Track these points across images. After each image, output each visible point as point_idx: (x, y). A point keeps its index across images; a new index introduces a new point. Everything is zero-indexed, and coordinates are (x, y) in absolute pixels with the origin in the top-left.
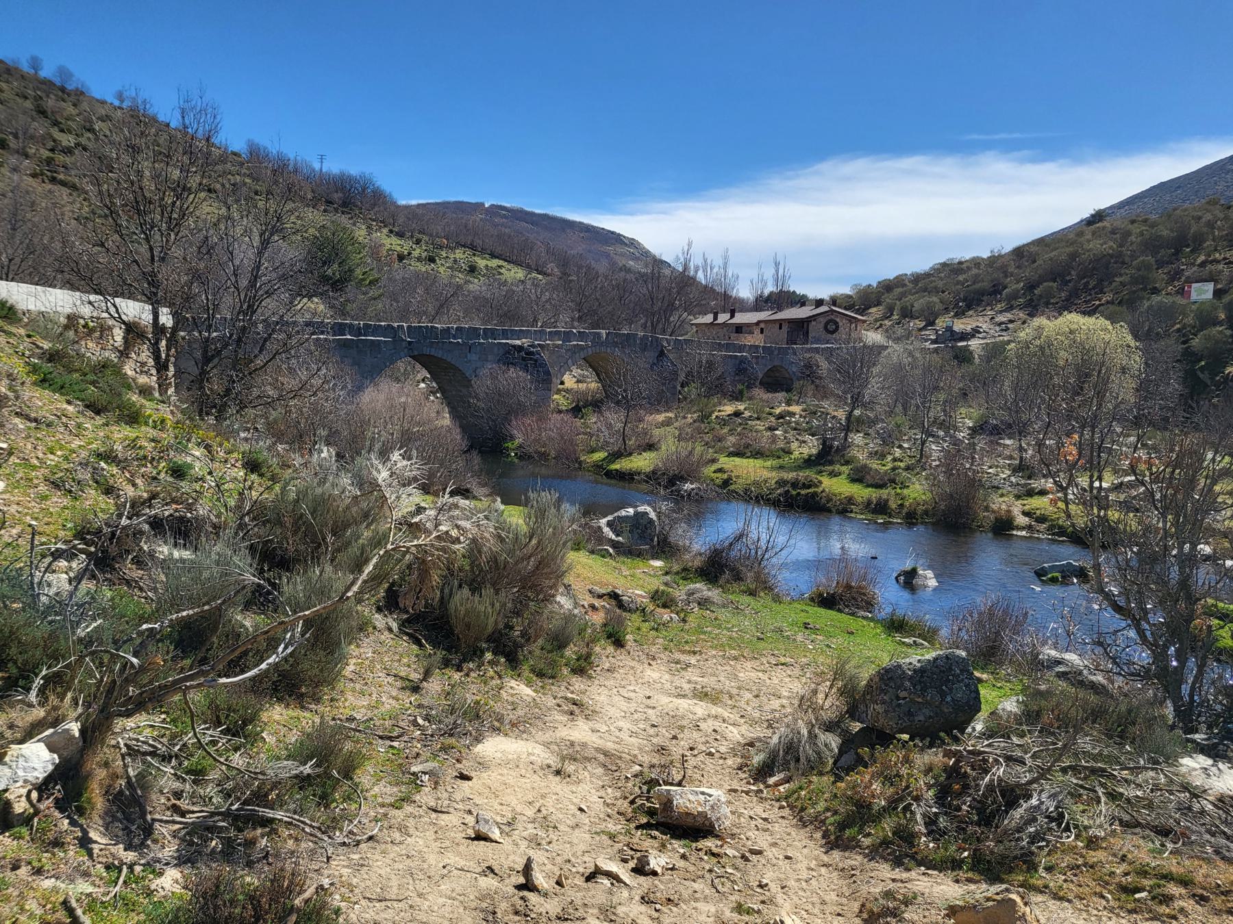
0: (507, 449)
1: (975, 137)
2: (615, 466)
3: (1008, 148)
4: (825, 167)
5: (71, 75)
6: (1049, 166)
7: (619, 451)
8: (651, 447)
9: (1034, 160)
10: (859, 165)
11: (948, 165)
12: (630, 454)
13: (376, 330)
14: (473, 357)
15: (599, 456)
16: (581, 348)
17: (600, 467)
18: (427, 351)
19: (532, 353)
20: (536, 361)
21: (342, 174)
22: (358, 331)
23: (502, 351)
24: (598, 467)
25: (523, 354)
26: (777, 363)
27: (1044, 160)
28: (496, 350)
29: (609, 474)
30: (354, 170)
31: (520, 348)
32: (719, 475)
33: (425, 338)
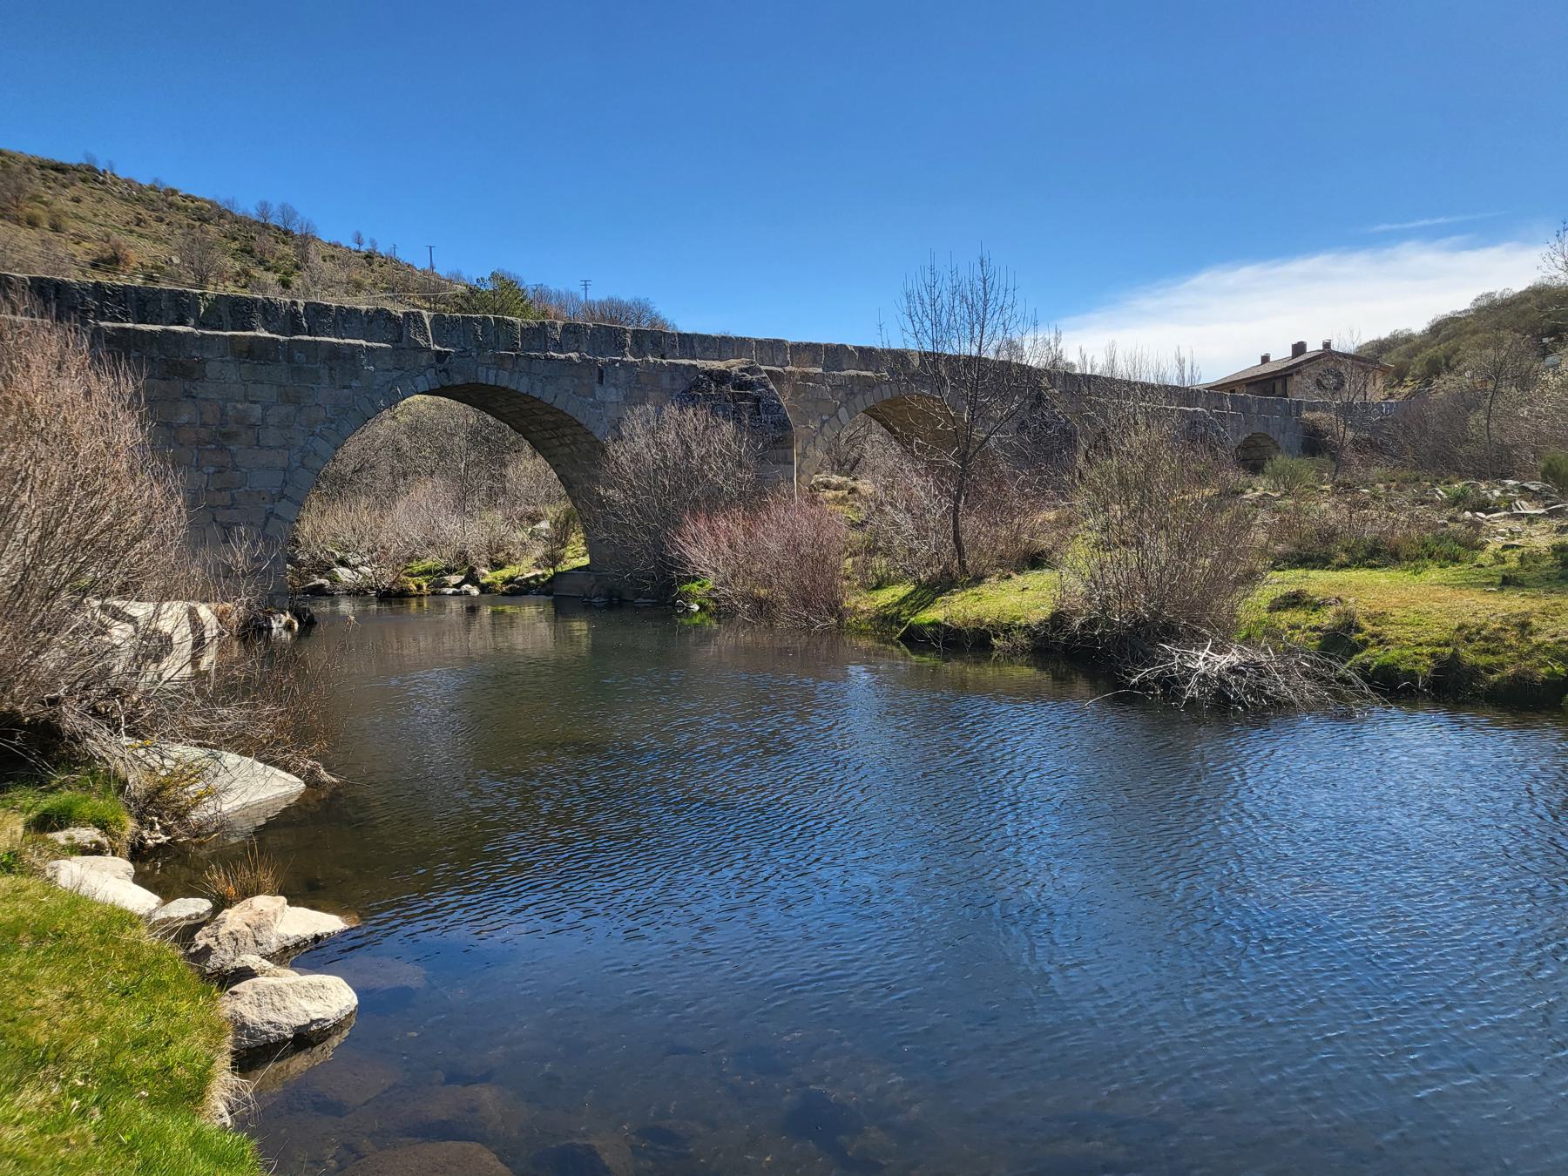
0: (687, 596)
1: (1385, 227)
2: (934, 614)
3: (1432, 235)
4: (1203, 279)
5: (295, 213)
6: (1493, 253)
7: (946, 572)
8: (1035, 561)
9: (1469, 247)
10: (1248, 273)
11: (1356, 264)
12: (979, 580)
13: (345, 319)
14: (612, 395)
15: (887, 596)
16: (868, 385)
17: (895, 620)
18: (488, 377)
19: (749, 385)
20: (758, 400)
21: (611, 301)
22: (291, 321)
23: (680, 384)
24: (885, 620)
25: (729, 388)
26: (1258, 428)
27: (1485, 246)
28: (665, 380)
29: (915, 639)
30: (626, 297)
31: (722, 377)
32: (1298, 616)
33: (481, 347)
